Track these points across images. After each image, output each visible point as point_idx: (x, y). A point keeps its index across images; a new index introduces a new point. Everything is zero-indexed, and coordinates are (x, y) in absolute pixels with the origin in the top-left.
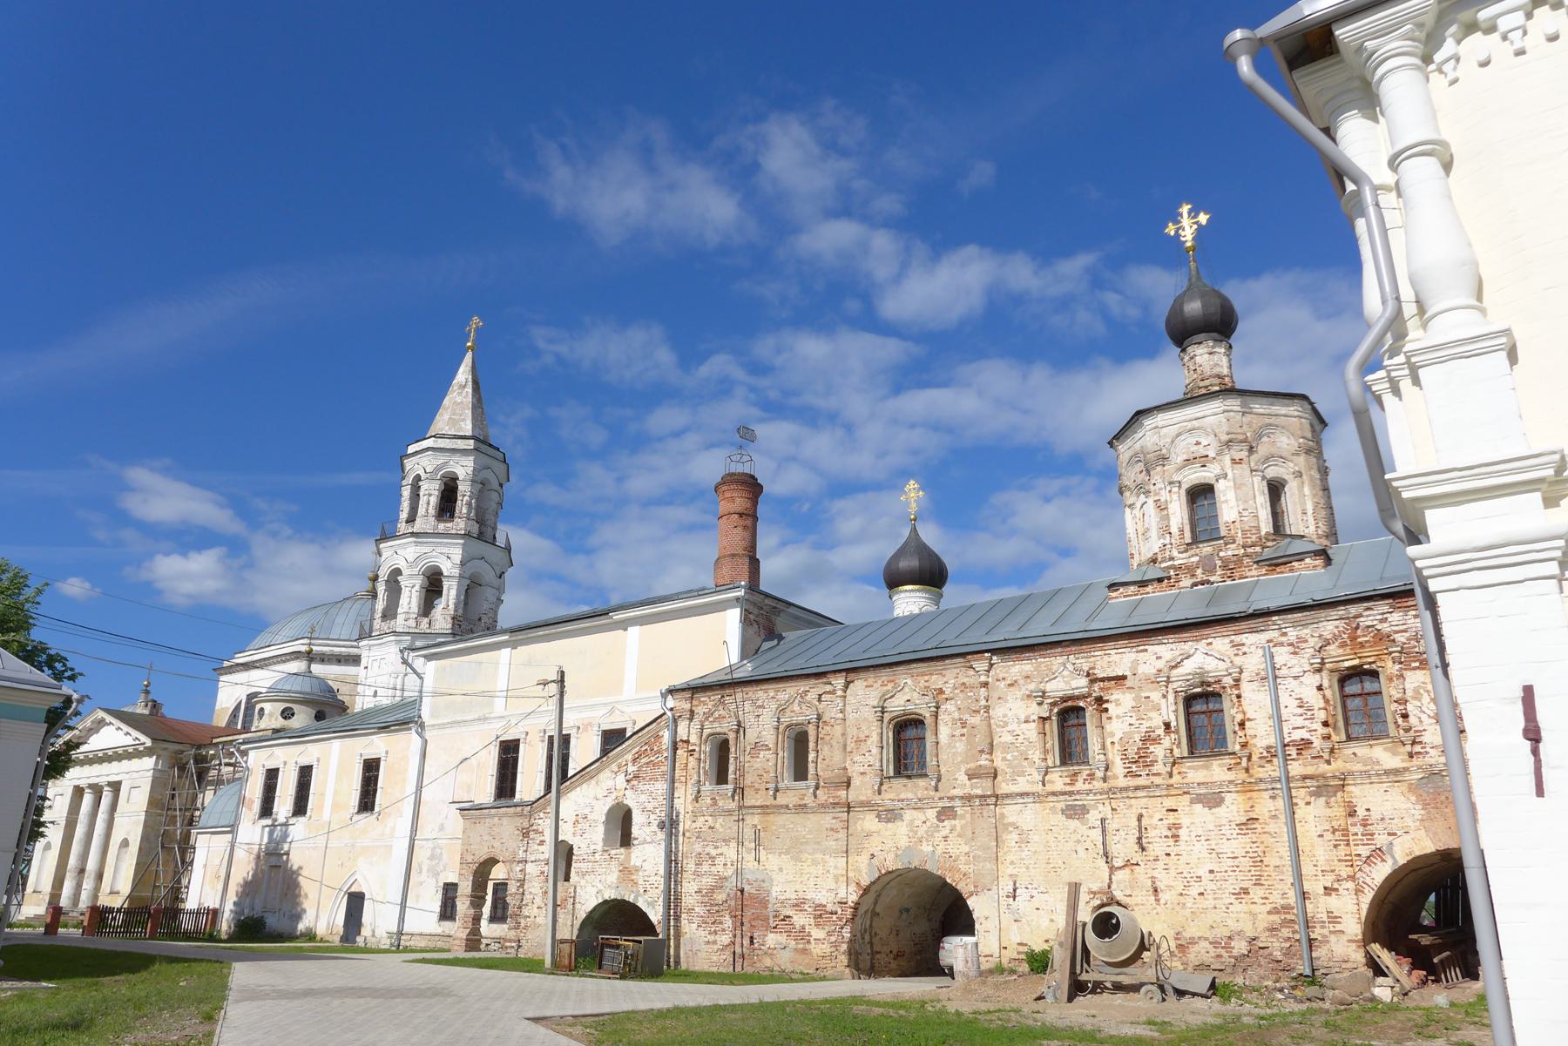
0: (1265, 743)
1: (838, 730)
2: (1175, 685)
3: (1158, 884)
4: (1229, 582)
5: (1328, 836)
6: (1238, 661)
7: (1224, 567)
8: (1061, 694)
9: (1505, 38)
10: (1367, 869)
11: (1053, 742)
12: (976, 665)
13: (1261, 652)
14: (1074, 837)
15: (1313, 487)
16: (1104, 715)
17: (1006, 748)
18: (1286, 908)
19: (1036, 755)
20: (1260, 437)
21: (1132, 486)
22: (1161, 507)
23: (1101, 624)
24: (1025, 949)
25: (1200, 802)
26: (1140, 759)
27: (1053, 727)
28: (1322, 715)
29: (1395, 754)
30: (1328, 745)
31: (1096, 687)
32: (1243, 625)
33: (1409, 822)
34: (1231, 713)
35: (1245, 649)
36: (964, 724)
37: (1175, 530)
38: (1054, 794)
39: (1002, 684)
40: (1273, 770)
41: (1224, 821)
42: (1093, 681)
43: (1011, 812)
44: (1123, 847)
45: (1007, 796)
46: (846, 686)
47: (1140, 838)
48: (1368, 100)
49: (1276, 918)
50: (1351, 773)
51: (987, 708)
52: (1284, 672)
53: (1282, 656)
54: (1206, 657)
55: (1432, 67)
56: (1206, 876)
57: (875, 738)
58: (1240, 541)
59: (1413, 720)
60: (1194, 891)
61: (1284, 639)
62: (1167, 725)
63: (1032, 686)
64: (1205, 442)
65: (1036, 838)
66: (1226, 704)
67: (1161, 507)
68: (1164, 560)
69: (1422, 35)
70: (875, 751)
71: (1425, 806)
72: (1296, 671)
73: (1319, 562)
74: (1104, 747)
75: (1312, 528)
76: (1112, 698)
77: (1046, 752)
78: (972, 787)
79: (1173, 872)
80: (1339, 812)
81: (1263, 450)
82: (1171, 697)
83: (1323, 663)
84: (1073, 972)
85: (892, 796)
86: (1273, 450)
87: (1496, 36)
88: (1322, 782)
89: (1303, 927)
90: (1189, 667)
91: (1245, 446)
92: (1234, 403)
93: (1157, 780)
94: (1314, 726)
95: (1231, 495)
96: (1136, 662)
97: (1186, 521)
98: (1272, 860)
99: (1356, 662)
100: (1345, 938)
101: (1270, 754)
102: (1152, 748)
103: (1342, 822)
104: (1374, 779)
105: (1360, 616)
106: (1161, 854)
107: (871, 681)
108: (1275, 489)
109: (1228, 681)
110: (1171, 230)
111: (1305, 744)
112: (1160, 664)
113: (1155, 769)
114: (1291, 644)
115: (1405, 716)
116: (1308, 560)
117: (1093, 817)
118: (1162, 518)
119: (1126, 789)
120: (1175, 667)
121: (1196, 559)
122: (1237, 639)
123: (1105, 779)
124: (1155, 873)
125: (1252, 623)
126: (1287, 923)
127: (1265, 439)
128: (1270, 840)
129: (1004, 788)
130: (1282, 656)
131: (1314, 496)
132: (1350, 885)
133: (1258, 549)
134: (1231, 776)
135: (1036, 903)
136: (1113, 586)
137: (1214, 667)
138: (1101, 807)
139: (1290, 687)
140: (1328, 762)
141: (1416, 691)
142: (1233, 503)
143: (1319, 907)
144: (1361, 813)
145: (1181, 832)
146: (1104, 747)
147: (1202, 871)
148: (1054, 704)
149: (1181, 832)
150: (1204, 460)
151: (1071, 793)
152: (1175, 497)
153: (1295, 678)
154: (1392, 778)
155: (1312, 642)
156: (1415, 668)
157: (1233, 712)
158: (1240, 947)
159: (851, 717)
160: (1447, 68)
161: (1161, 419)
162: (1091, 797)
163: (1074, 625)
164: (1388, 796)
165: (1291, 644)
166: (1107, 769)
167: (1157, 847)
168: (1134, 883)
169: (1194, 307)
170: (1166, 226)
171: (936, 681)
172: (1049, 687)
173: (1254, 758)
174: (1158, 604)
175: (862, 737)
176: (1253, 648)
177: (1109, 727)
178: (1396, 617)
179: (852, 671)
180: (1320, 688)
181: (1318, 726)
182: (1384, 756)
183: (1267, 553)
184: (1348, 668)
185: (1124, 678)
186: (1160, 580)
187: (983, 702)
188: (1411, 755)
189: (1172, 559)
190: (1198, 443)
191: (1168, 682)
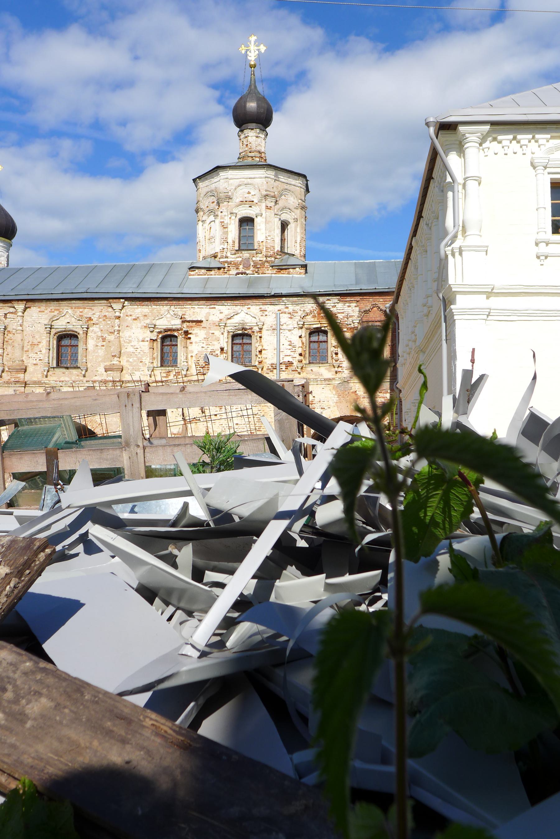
1: (18, 337)
2: (228, 328)
4: (256, 275)
6: (262, 319)
7: (255, 266)
8: (165, 327)
9: (503, 147)
11: (157, 354)
12: (114, 306)
13: (274, 315)
15: (302, 228)
16: (188, 341)
17: (130, 355)
19: (147, 360)
20: (281, 195)
21: (206, 210)
22: (224, 227)
23: (190, 289)
28: (300, 351)
29: (330, 371)
30: (300, 365)
31: (185, 325)
32: (268, 300)
33: (331, 403)
34: (255, 345)
35: (266, 313)
36: (104, 340)
37: (230, 241)
46: (25, 310)
48: (460, 149)
51: (119, 331)
52: (284, 327)
53: (284, 318)
54: (246, 315)
55: (481, 148)
57: (44, 343)
58: (264, 253)
61: (286, 310)
62: (222, 349)
63: (148, 321)
64: (253, 193)
66: (254, 340)
67: (224, 227)
69: (481, 137)
70: (44, 351)
71: (339, 396)
72: (290, 327)
73: (303, 271)
74: (187, 358)
75: (298, 251)
76: (193, 332)
78: (107, 376)
81: (281, 203)
82: (226, 334)
83: (303, 325)
85: (55, 379)
86: (287, 205)
87: (500, 145)
90: (236, 320)
91: (274, 200)
92: (271, 173)
96: (209, 314)
97: (237, 237)
99: (319, 326)
107: (43, 308)
108: (284, 226)
109: (256, 329)
111: (290, 364)
112: (222, 316)
114: (290, 313)
116: (297, 269)
120: (230, 318)
121: (240, 259)
122: (264, 307)
125: (272, 300)
127: (283, 197)
130: (284, 318)
131: (302, 233)
136: (192, 268)
137: (250, 321)
139: (286, 335)
140: (299, 373)
142: (263, 231)
146: (187, 358)
148: (160, 333)
152: (233, 222)
155: (300, 313)
157: (257, 345)
159: (28, 330)
160: (486, 150)
161: (230, 173)
163: (171, 289)
165: (290, 313)
166: (187, 370)
169: (252, 105)
171: (87, 313)
172: (158, 323)
173: (265, 369)
174: (220, 283)
175: (36, 342)
176: (270, 313)
177: (190, 348)
178: (340, 305)
179: (30, 301)
180: (300, 337)
181: (297, 355)
183: (277, 262)
184: (314, 328)
185: (201, 322)
186: (219, 268)
187: (117, 328)
188: (336, 372)
189: (227, 257)
190: (249, 193)
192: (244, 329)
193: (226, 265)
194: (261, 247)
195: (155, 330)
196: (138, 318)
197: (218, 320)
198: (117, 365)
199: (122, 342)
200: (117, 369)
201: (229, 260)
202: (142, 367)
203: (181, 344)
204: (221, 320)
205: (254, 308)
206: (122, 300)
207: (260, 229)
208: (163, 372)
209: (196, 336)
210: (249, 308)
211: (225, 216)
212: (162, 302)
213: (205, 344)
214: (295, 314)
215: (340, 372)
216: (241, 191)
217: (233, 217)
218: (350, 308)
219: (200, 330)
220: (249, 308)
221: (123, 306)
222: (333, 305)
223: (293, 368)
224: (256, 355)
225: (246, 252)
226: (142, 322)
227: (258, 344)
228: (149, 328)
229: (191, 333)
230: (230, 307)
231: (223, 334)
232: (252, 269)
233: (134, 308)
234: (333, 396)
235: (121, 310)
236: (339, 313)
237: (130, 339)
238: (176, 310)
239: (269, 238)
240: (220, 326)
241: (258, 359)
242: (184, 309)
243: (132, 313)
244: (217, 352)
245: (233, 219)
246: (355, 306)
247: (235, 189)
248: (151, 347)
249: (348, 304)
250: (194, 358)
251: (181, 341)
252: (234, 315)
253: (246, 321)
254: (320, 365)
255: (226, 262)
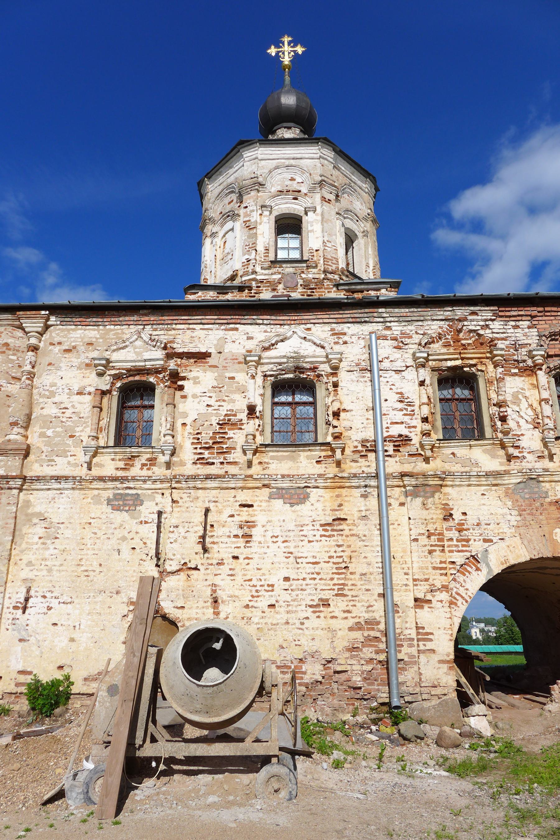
0: (361, 436)
2: (265, 368)
3: (219, 593)
5: (423, 540)
8: (128, 365)
10: (461, 578)
11: (109, 419)
12: (28, 325)
14: (119, 533)
16: (178, 394)
17: (48, 422)
18: (371, 623)
19: (85, 433)
22: (250, 227)
24: (28, 679)
25: (281, 497)
26: (215, 445)
27: (112, 403)
29: (494, 456)
32: (348, 314)
33: (504, 528)
35: (346, 338)
37: (260, 248)
38: (101, 479)
39: (57, 349)
40: (368, 465)
41: (307, 521)
42: (169, 356)
43: (38, 500)
44: (180, 547)
45: (38, 479)
47: (203, 537)
49: (358, 635)
50: (451, 474)
51: (31, 376)
52: (386, 364)
56: (280, 585)
59: (511, 424)
60: (263, 603)
61: (388, 332)
62: (251, 409)
63: (95, 354)
65: (68, 533)
66: (320, 392)
67: (250, 227)
68: (246, 274)
72: (399, 365)
74: (173, 427)
76: (190, 375)
77: (99, 429)
79: (239, 579)
80: (439, 514)
82: (259, 379)
84: (131, 744)
86: (350, 207)
88: (421, 481)
89: (384, 645)
90: (283, 349)
93: (232, 470)
94: (414, 423)
95: (317, 227)
98: (357, 567)
99: (458, 363)
100: (435, 658)
101: (369, 448)
102: (230, 434)
103: (438, 526)
104: (474, 481)
105: (465, 319)
106: (227, 556)
109: (325, 368)
110: (272, 51)
111: (404, 440)
112: (251, 345)
113: (231, 457)
115: (503, 419)
117: (148, 510)
118: (249, 237)
119: (195, 477)
122: (339, 328)
123: (168, 465)
124: (217, 580)
125: (356, 313)
126: (370, 641)
128: (357, 544)
129: (35, 468)
130: (385, 349)
132: (444, 596)
133: (336, 277)
134: (319, 469)
135: (53, 616)
137: (309, 352)
138: (158, 498)
140: (427, 460)
141: (515, 396)
142: (319, 233)
143: (406, 623)
144: (457, 516)
145: (254, 531)
147: (276, 579)
148: (117, 377)
149: (254, 531)
150: (296, 194)
151: (123, 479)
153: (398, 372)
154: (492, 480)
155: (416, 338)
156: (515, 375)
157: (329, 400)
158: (313, 671)
162: (149, 485)
164: (484, 500)
166: (173, 454)
167: (223, 548)
168: (189, 593)
170: (269, 48)
172: (115, 356)
173: (348, 451)
176: (354, 339)
177: (182, 407)
178: (497, 325)
181: (417, 422)
182: (482, 457)
187: (28, 368)
191: (258, 363)
192: (298, 369)
193: (254, 284)
194: (315, 259)
195: (108, 372)
196: (74, 347)
197: (244, 351)
198: (16, 442)
199: (35, 397)
200: (14, 452)
201: (259, 277)
202: (72, 448)
203: (162, 397)
204: (250, 351)
205: (321, 330)
206: (43, 312)
207: (312, 231)
208: (118, 457)
209: (195, 383)
210: (309, 329)
211: (253, 211)
212: (127, 318)
213: (214, 399)
214: (407, 341)
215: (517, 457)
216: (279, 177)
217: (267, 213)
218: (519, 330)
219: (205, 371)
220: (309, 329)
221: (47, 327)
222: (482, 323)
223: (413, 450)
224: (328, 423)
225: (289, 265)
226: (83, 356)
227: (331, 398)
228: (96, 366)
229: (184, 378)
230: (268, 328)
231: (253, 377)
232: (300, 289)
233: (68, 330)
234: (508, 512)
235: (42, 335)
236: (498, 339)
237: (53, 388)
238: (155, 333)
239: (329, 244)
240: (246, 362)
241: (331, 430)
242: (173, 332)
243: (62, 340)
244: (239, 416)
245: (266, 216)
246: (529, 327)
247: (270, 172)
248: (97, 404)
249: (513, 323)
250: (188, 427)
251: (163, 393)
252: (276, 343)
253: (303, 353)
254: (473, 443)
255: (254, 280)
